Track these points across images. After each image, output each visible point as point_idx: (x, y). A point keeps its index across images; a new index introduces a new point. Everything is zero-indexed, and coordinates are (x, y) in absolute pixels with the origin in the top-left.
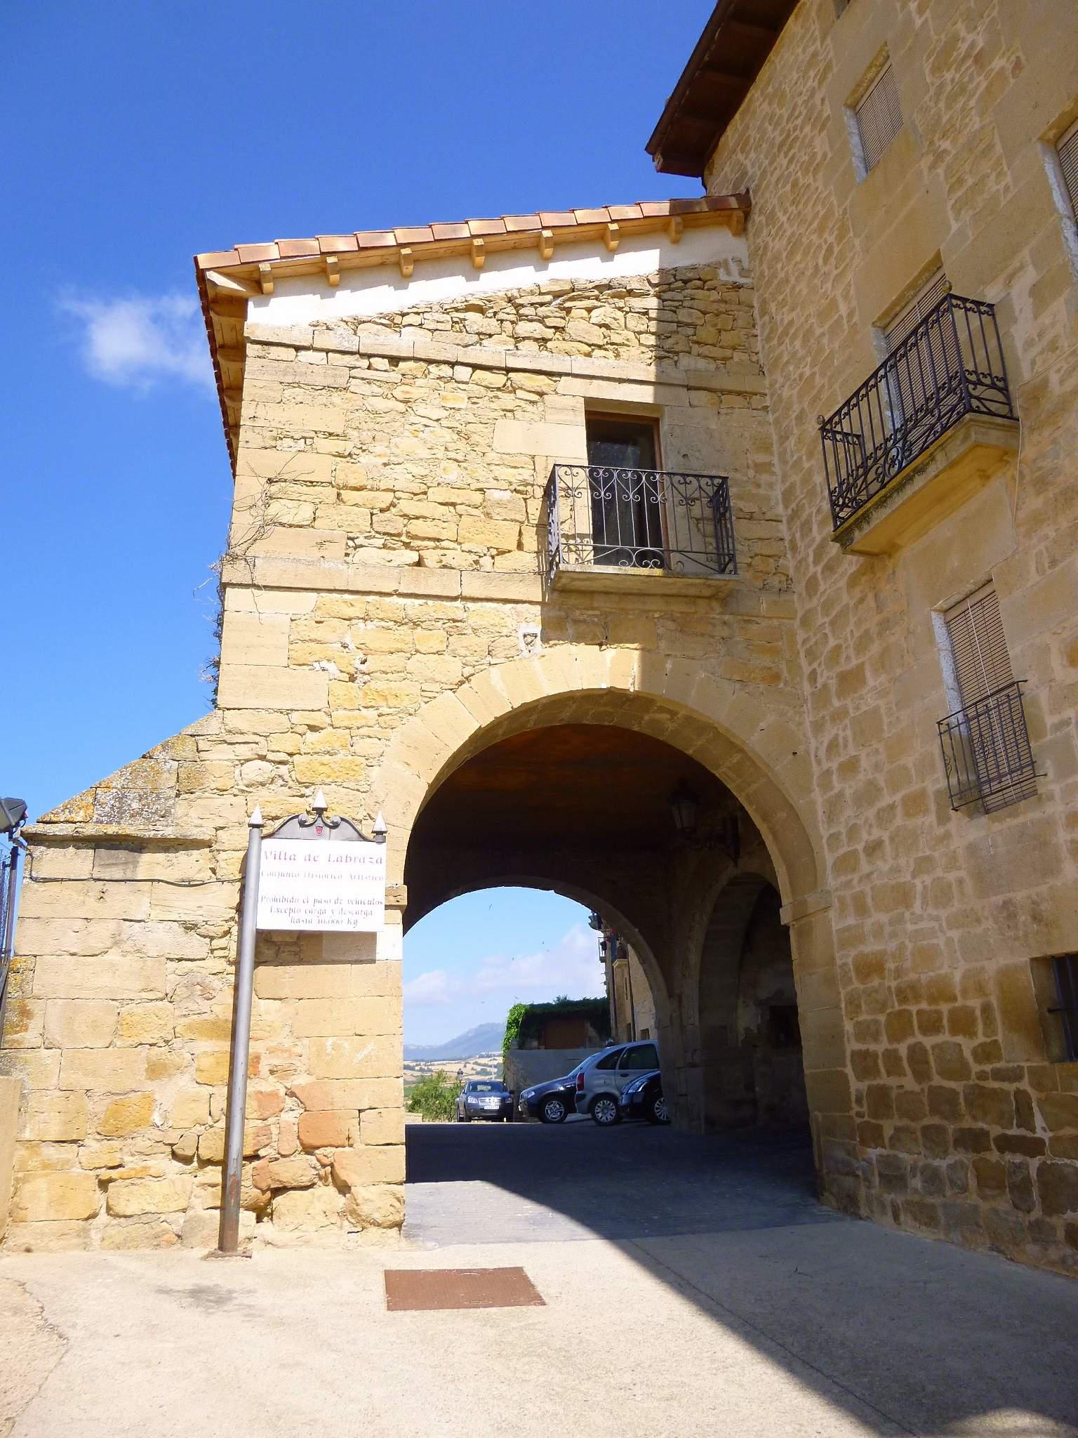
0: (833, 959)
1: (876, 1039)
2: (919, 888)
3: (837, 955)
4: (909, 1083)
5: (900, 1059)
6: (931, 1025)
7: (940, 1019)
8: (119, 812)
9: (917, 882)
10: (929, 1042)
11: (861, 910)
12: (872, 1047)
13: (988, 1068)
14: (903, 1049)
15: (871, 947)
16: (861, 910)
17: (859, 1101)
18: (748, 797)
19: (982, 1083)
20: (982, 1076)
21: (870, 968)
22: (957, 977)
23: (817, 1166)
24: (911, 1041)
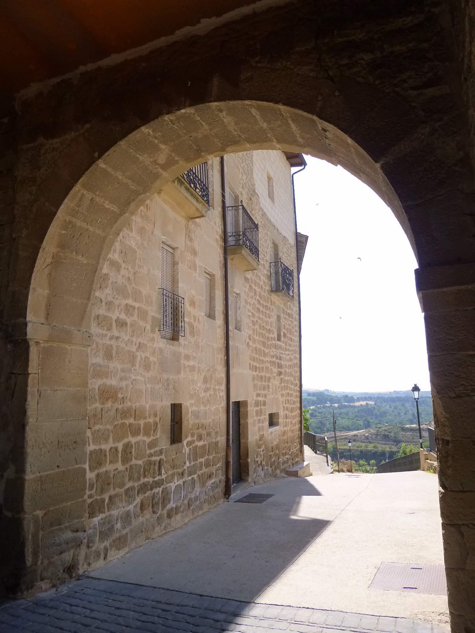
0: (87, 383)
1: (106, 440)
2: (139, 358)
3: (90, 382)
4: (120, 466)
5: (87, 454)
6: (136, 432)
7: (139, 428)
8: (414, 407)
9: (138, 354)
10: (133, 440)
11: (109, 356)
12: (103, 447)
13: (152, 451)
14: (120, 446)
15: (113, 382)
16: (109, 356)
17: (91, 487)
18: (66, 225)
19: (150, 459)
20: (151, 455)
21: (108, 394)
22: (147, 406)
23: (29, 564)
24: (125, 441)
